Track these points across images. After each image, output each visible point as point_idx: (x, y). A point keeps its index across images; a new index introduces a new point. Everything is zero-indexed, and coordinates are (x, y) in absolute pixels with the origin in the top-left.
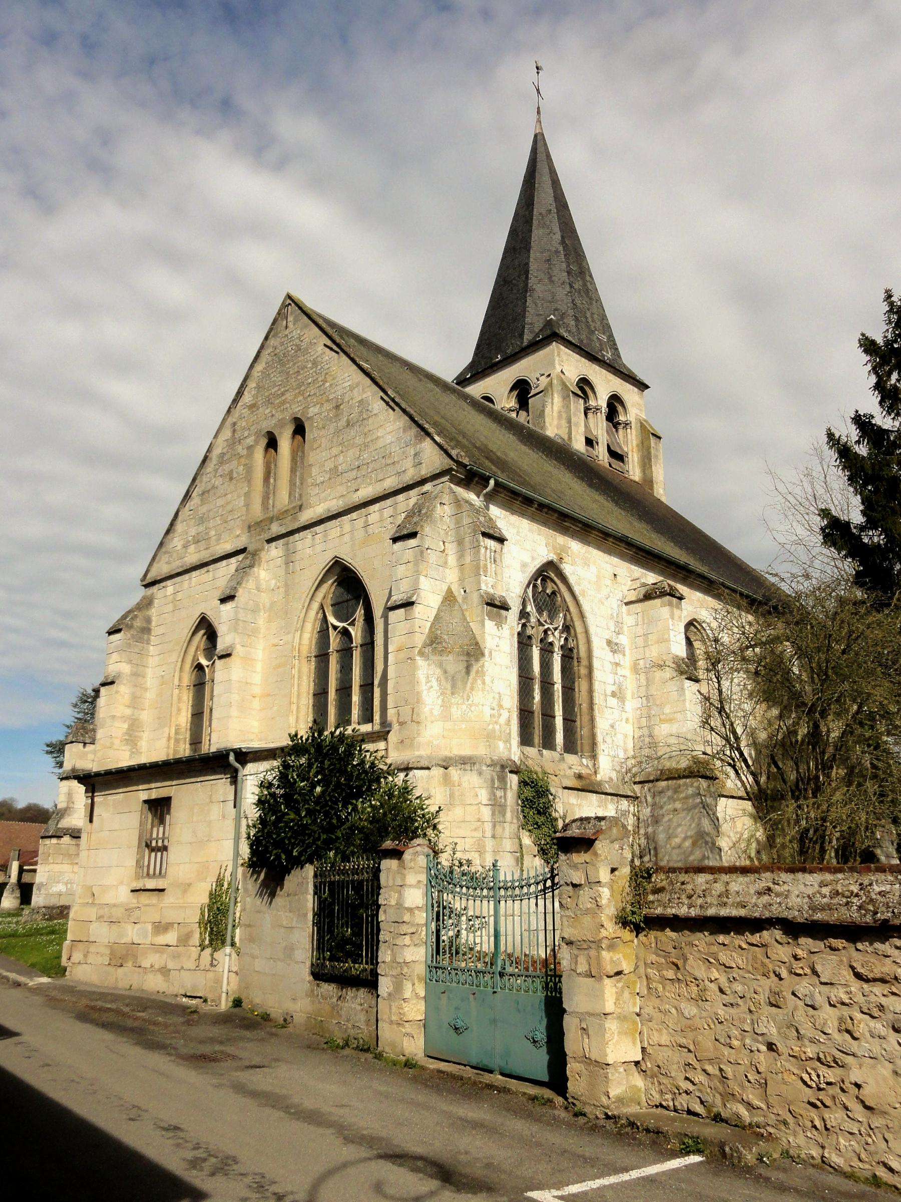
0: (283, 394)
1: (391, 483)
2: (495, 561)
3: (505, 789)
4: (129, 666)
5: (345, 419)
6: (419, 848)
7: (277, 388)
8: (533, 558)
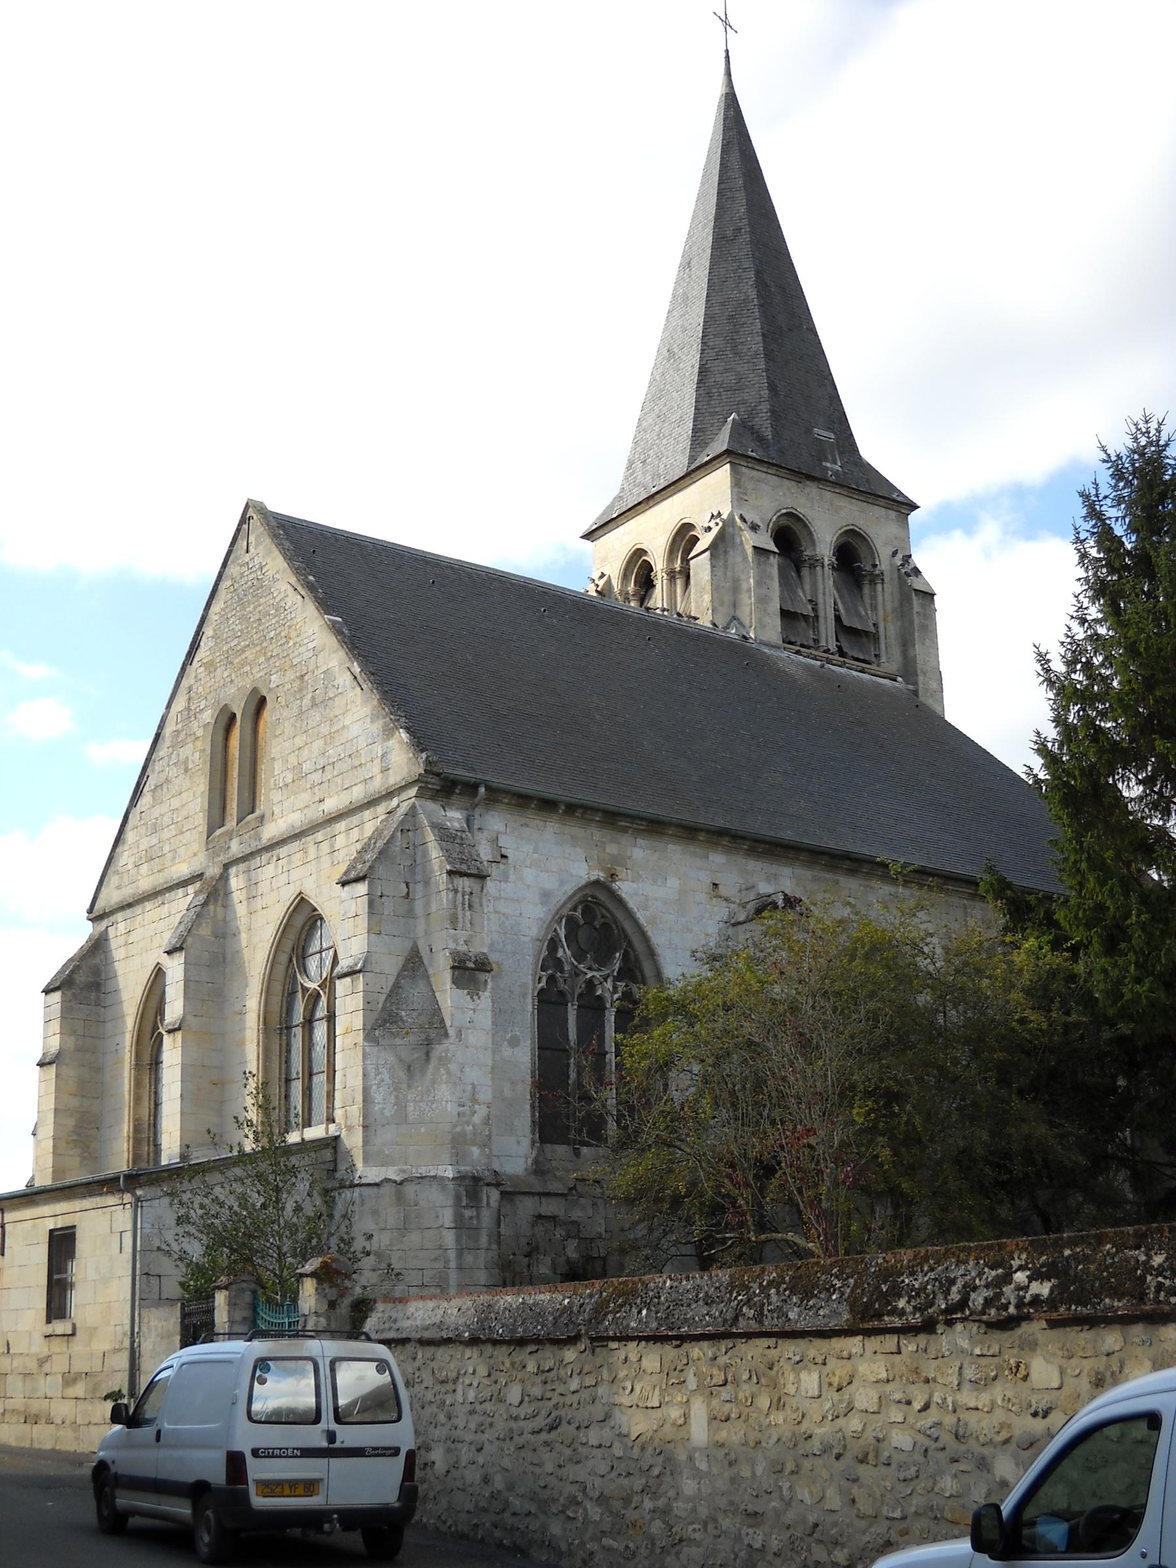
0: (243, 651)
1: (358, 794)
2: (470, 906)
3: (478, 1208)
4: (73, 1038)
5: (310, 696)
6: (244, 1285)
7: (235, 642)
8: (562, 882)
